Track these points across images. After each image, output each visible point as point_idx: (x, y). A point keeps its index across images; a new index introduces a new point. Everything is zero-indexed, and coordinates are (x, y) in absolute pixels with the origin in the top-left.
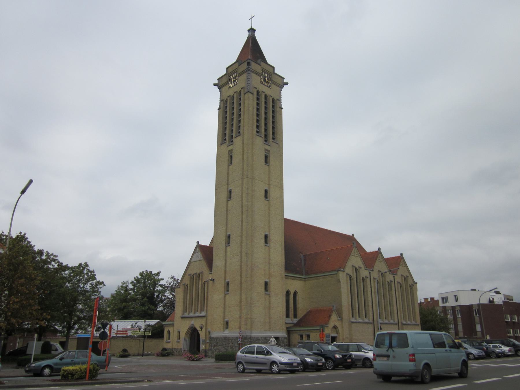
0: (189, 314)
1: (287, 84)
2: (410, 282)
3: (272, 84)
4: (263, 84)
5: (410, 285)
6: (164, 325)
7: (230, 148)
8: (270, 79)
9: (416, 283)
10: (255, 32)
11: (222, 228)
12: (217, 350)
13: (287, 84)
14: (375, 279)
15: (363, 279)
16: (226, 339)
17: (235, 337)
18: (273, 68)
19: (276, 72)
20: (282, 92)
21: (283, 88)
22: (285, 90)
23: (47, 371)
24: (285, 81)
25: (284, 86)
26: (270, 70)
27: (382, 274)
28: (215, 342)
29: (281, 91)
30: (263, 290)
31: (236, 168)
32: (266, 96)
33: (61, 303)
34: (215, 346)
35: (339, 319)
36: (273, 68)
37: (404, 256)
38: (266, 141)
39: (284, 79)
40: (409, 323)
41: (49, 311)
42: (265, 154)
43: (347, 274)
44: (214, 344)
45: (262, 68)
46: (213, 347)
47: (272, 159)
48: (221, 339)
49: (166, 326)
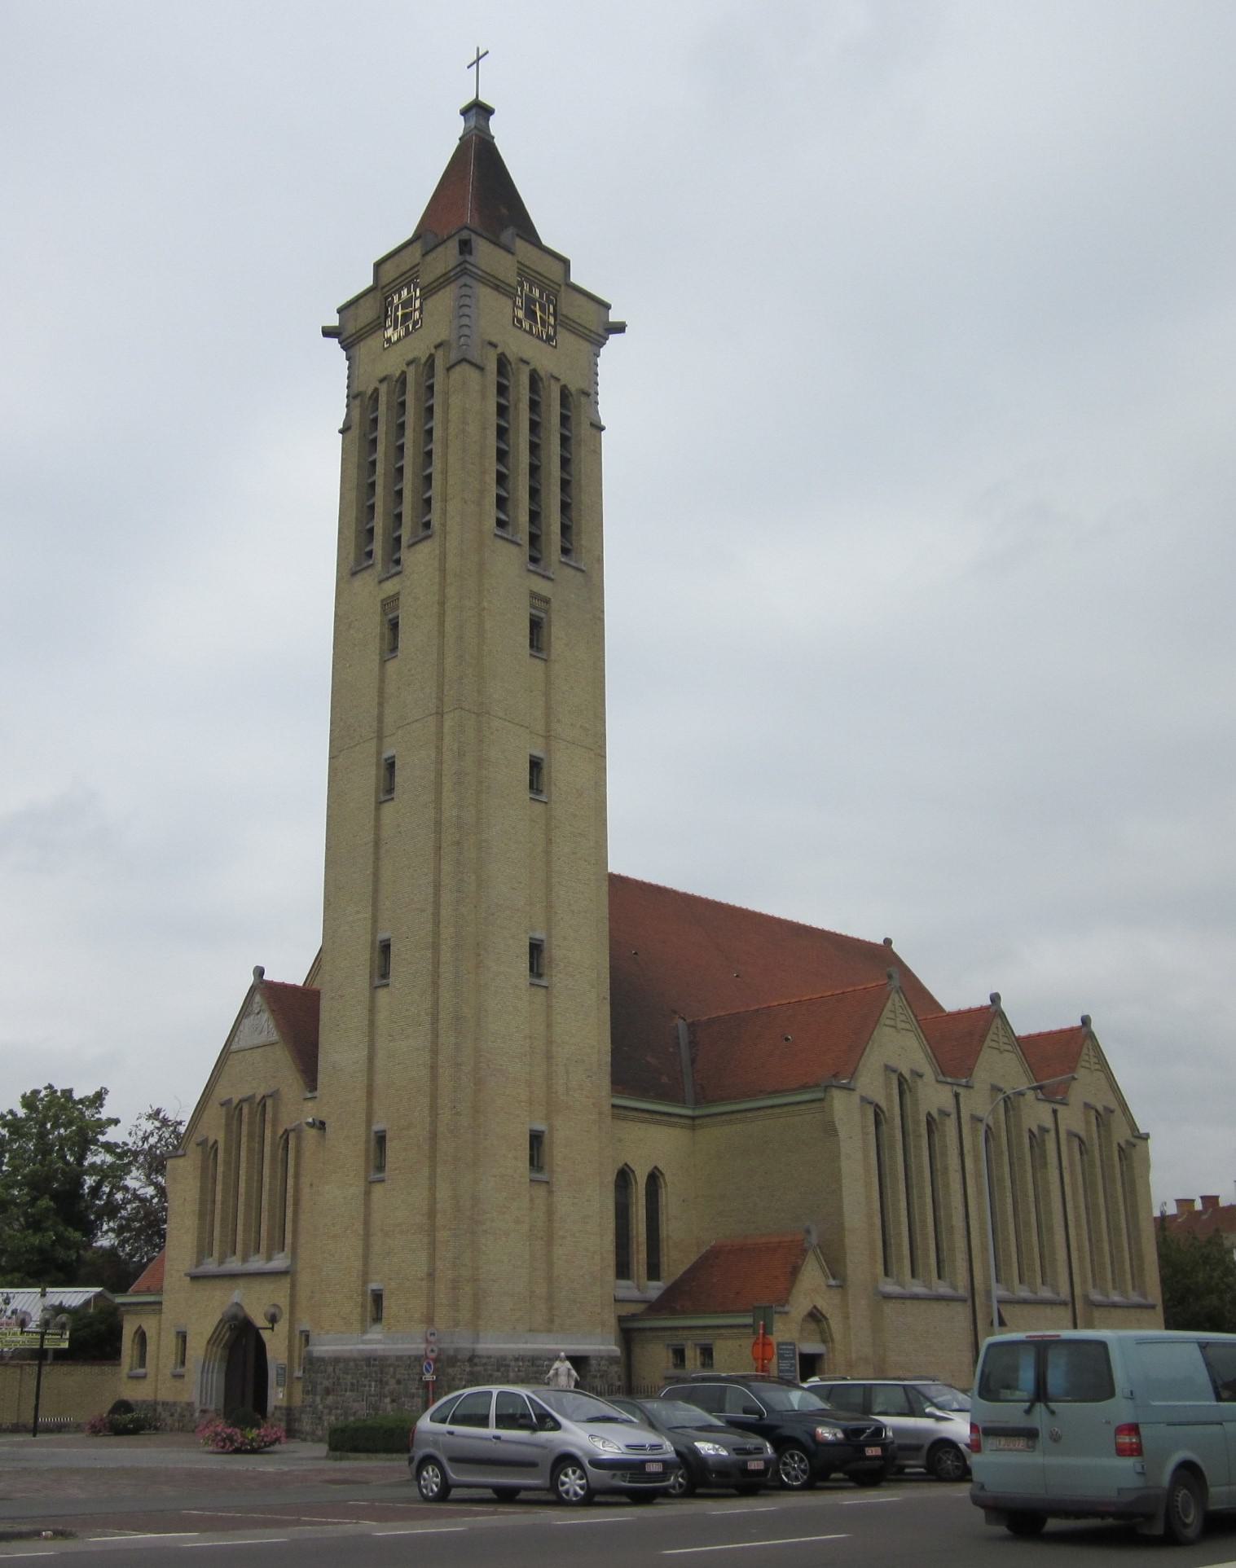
0: (221, 1262)
1: (620, 328)
2: (1120, 1135)
3: (558, 328)
7: (390, 587)
11: (358, 912)
12: (337, 1408)
13: (620, 328)
15: (930, 1121)
16: (372, 1362)
17: (410, 1357)
18: (561, 264)
22: (612, 356)
24: (614, 317)
26: (553, 271)
32: (535, 379)
34: (328, 1392)
35: (832, 1282)
36: (565, 263)
38: (534, 560)
39: (607, 307)
42: (531, 614)
44: (326, 1383)
45: (518, 262)
46: (318, 1399)
47: (558, 633)
49: (128, 1312)
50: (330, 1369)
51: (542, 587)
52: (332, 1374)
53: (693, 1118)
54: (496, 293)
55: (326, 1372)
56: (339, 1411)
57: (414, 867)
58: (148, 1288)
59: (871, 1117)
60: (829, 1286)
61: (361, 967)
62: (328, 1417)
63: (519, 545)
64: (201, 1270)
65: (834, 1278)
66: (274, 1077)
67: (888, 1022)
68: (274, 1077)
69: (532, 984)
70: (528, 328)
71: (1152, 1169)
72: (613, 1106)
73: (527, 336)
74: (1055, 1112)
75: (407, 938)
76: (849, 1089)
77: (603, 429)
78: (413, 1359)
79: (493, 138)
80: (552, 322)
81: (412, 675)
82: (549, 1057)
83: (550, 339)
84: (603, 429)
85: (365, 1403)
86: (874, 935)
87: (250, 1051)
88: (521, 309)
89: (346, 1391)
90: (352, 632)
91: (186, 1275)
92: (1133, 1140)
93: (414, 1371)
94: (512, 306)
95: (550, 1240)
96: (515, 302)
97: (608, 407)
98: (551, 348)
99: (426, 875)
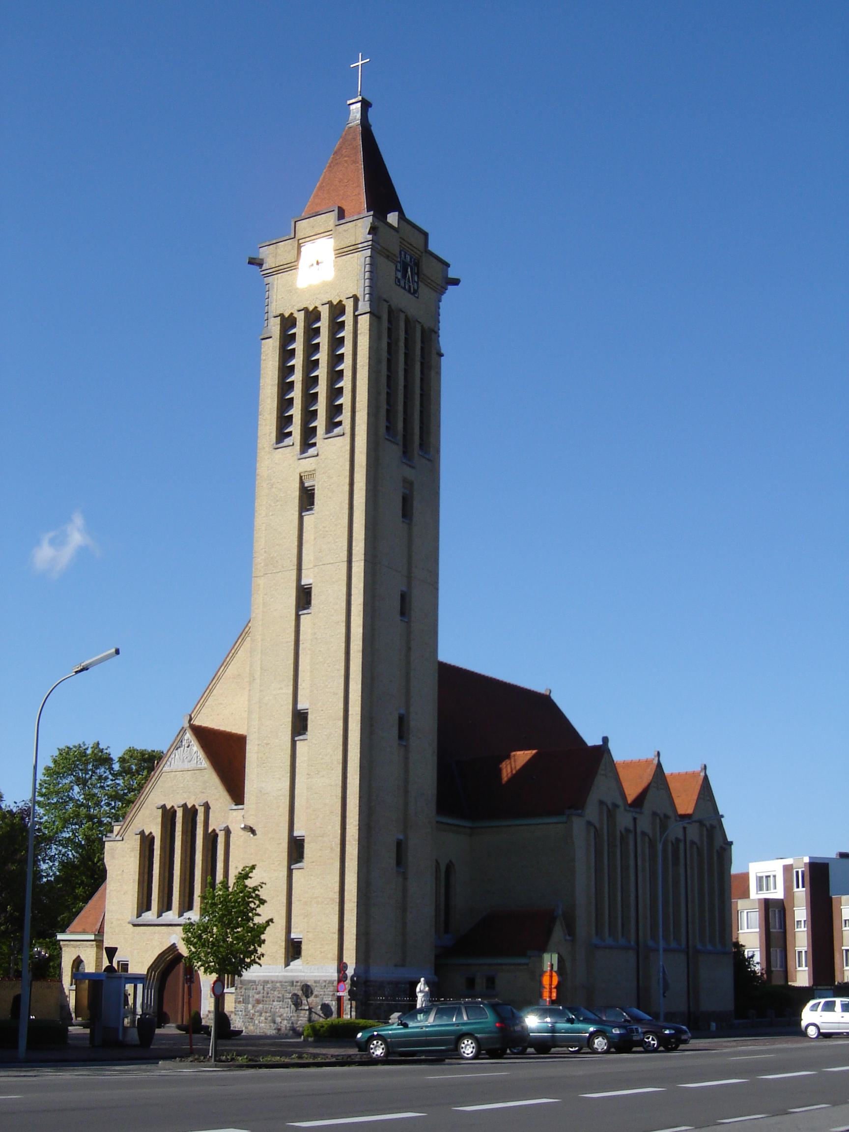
0: (160, 915)
1: (456, 282)
2: (718, 843)
3: (420, 283)
4: (402, 287)
5: (620, 831)
6: (61, 943)
7: (307, 465)
8: (416, 271)
9: (731, 843)
10: (370, 109)
11: (281, 688)
12: (266, 1012)
13: (456, 282)
14: (644, 834)
15: (622, 837)
16: (295, 984)
17: (325, 981)
18: (423, 236)
19: (433, 247)
20: (441, 303)
21: (443, 293)
22: (450, 299)
23: (329, 1056)
24: (452, 274)
25: (446, 289)
26: (417, 241)
27: (609, 811)
28: (259, 993)
29: (440, 301)
30: (393, 862)
31: (327, 529)
32: (407, 321)
33: (225, 919)
34: (258, 1002)
35: (568, 938)
36: (426, 235)
37: (611, 746)
38: (404, 453)
39: (448, 265)
40: (709, 947)
41: (211, 939)
42: (403, 493)
43: (589, 823)
44: (257, 996)
45: (401, 238)
46: (250, 1006)
47: (417, 506)
48: (278, 985)
49: (67, 946)
50: (260, 988)
51: (409, 473)
52: (262, 991)
53: (470, 828)
54: (386, 261)
55: (256, 989)
56: (268, 1014)
57: (328, 664)
58: (84, 929)
59: (592, 834)
60: (566, 940)
61: (283, 726)
62: (259, 1018)
63: (397, 444)
64: (140, 921)
65: (569, 935)
66: (203, 792)
67: (603, 772)
68: (203, 792)
69: (399, 744)
70: (403, 286)
71: (732, 864)
72: (437, 822)
73: (403, 291)
74: (685, 829)
75: (322, 710)
76: (580, 815)
77: (442, 355)
78: (327, 982)
79: (371, 126)
80: (416, 280)
81: (327, 531)
82: (406, 792)
83: (415, 292)
84: (442, 355)
85: (289, 1009)
86: (540, 689)
87: (181, 773)
88: (400, 271)
89: (273, 1001)
90: (274, 490)
91: (129, 923)
92: (724, 846)
93: (328, 990)
94: (394, 269)
95: (404, 909)
96: (396, 267)
97: (446, 340)
98: (414, 298)
99: (338, 670)
